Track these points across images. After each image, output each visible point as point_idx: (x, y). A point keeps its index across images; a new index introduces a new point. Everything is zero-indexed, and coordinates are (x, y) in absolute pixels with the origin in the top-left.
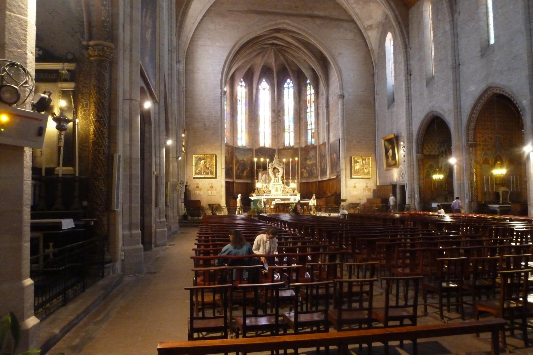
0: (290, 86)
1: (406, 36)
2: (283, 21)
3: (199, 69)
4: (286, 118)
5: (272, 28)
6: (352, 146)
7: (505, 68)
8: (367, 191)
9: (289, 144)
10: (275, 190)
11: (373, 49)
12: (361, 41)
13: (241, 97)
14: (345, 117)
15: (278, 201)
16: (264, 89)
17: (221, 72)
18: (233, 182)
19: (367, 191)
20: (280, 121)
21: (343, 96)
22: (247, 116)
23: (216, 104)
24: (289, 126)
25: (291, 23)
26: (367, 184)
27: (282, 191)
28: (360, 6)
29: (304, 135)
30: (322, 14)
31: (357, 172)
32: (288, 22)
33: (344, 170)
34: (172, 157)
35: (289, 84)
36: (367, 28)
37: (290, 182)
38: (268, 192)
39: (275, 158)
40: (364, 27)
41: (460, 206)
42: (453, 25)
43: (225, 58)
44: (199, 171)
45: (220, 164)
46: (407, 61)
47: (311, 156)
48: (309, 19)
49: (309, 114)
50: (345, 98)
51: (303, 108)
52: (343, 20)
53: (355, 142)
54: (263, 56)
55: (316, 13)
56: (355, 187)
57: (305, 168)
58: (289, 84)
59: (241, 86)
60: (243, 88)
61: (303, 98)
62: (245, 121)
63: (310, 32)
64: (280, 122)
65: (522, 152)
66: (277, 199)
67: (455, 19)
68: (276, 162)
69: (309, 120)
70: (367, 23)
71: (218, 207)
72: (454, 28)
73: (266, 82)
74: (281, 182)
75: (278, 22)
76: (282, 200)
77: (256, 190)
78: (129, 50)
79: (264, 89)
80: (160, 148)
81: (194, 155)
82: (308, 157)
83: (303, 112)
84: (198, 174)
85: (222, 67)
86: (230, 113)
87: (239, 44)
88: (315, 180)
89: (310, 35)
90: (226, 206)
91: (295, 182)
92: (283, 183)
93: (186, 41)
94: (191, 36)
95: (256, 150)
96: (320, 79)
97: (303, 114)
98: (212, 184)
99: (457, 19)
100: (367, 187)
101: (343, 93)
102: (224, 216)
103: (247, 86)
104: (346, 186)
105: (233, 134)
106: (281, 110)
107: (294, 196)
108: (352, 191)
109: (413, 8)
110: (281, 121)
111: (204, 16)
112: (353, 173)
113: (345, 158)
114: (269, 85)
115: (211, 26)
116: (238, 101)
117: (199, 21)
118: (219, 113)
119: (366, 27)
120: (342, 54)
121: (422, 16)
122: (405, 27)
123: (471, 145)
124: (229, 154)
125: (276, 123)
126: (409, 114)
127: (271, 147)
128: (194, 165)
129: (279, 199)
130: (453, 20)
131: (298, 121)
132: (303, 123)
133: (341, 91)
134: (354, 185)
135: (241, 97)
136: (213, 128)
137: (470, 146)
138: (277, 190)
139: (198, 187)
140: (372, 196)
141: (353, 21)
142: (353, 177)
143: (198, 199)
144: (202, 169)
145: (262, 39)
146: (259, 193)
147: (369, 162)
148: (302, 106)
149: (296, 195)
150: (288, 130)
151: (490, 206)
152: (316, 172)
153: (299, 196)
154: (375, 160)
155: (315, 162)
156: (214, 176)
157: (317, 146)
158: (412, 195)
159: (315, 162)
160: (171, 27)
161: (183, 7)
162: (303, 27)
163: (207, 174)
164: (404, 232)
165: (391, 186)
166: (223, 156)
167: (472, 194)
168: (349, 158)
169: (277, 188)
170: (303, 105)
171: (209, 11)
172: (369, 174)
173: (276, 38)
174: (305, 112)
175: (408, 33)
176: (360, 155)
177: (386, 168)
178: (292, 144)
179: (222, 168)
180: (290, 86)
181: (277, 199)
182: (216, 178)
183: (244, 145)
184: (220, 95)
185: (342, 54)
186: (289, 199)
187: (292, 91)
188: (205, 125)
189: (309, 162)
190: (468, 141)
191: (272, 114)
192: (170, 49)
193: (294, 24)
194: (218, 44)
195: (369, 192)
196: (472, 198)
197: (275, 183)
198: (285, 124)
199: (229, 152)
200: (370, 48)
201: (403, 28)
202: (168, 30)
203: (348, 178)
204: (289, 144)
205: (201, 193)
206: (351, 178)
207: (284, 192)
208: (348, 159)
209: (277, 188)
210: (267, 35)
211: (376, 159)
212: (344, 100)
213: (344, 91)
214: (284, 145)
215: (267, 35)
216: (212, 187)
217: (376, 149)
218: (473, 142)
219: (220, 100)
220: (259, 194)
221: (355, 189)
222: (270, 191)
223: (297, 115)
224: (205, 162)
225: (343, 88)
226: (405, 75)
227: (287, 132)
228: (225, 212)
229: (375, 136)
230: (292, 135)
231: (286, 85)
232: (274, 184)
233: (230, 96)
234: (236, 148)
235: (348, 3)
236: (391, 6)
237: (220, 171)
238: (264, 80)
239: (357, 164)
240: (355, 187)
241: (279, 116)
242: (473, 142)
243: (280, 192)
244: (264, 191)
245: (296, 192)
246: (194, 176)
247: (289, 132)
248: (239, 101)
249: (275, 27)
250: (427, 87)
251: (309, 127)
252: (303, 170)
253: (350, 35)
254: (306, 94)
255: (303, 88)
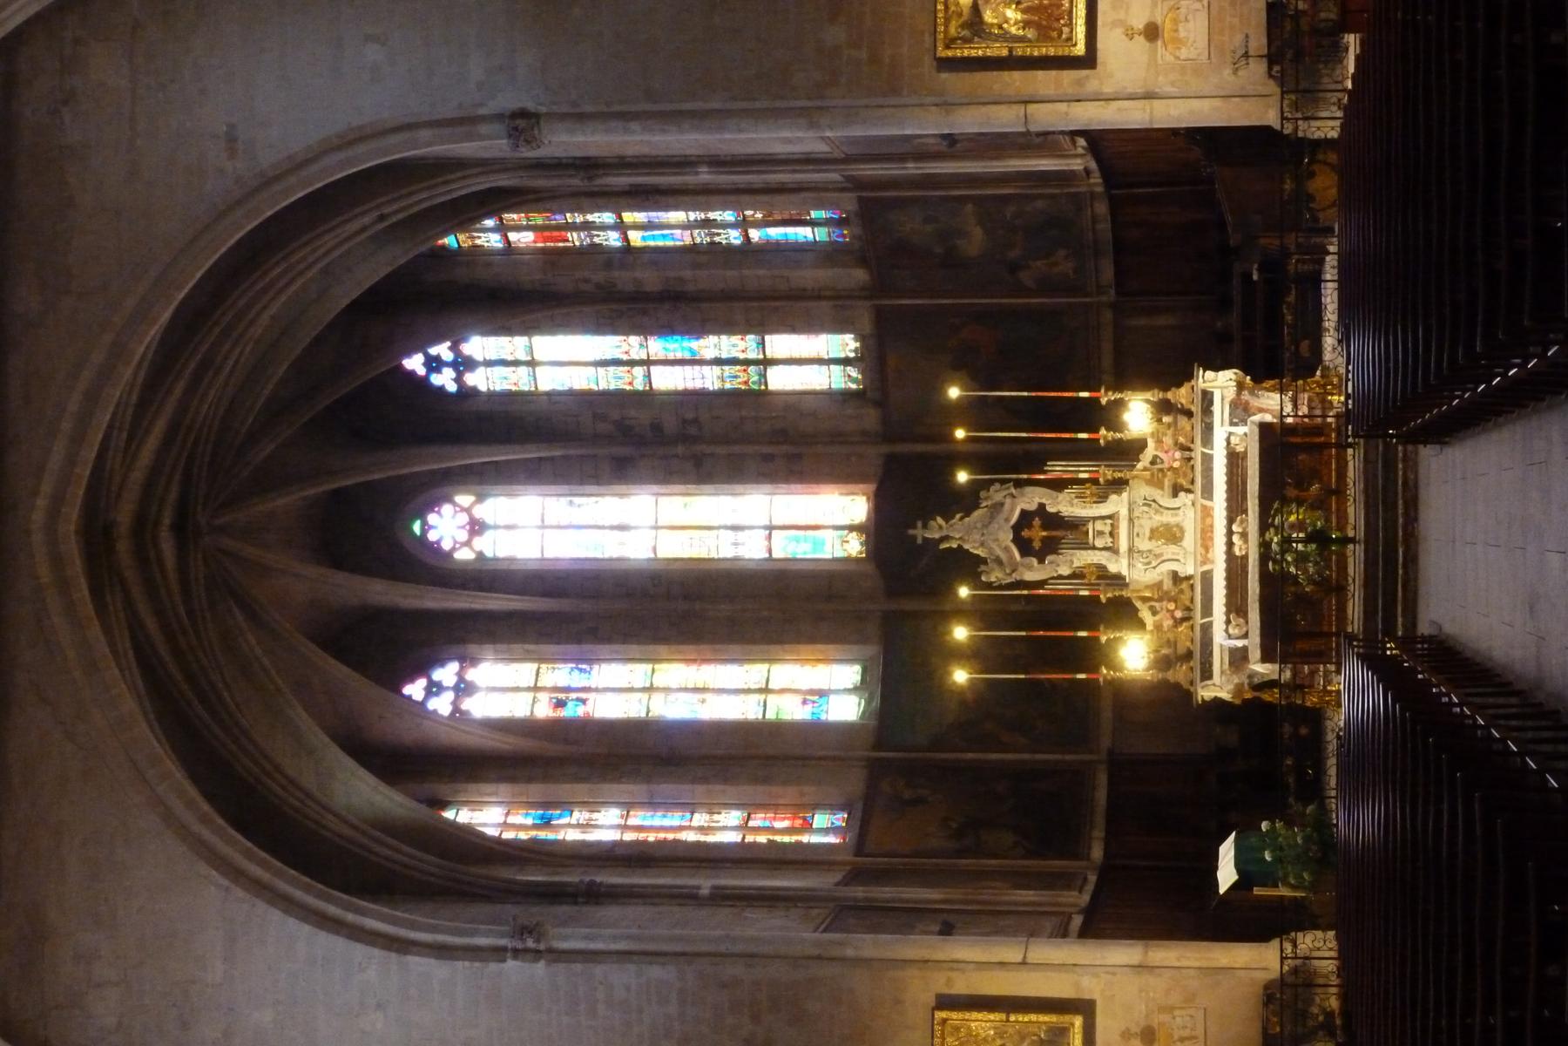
2: (38, 538)
6: (864, 54)
13: (536, 689)
15: (1244, 535)
21: (521, 123)
22: (662, 650)
23: (601, 994)
25: (47, 487)
27: (1175, 495)
29: (786, 273)
31: (1047, 20)
33: (1032, 108)
35: (434, 364)
38: (1185, 598)
39: (946, 538)
45: (1002, 975)
47: (929, 228)
50: (530, 106)
51: (600, 277)
53: (835, 34)
56: (1152, 32)
57: (1014, 268)
58: (434, 364)
60: (472, 675)
62: (693, 668)
65: (950, 682)
69: (683, 238)
73: (432, 518)
75: (44, 573)
79: (476, 527)
82: (938, 250)
83: (624, 279)
86: (648, 780)
88: (1102, 208)
90: (1275, 943)
91: (1119, 405)
92: (1118, 485)
95: (891, 593)
97: (638, 274)
104: (1149, 96)
110: (690, 416)
112: (1052, 52)
113: (947, 105)
118: (656, 972)
125: (708, 449)
132: (705, 279)
133: (484, 129)
134: (1140, 40)
135: (536, 689)
136: (756, 1018)
138: (1172, 535)
148: (586, 281)
149: (1207, 397)
150: (752, 369)
152: (1040, 204)
153: (1210, 374)
155: (969, 207)
156: (1078, 1021)
157: (860, 199)
159: (969, 207)
166: (940, 956)
168: (944, 76)
169: (1154, 534)
170: (578, 275)
179: (1024, 963)
181: (1230, 544)
182: (1085, 1008)
184: (541, 965)
189: (974, 241)
197: (1123, 545)
199: (907, 794)
203: (1091, 81)
206: (1089, 60)
207: (1183, 482)
208: (953, 81)
209: (1154, 534)
212: (543, 109)
213: (483, 111)
219: (578, 967)
220: (1196, 662)
223: (645, 312)
225: (462, 121)
227: (763, 376)
232: (1131, 550)
233: (530, 780)
234: (879, 745)
239: (989, 16)
240: (1152, 32)
241: (657, 428)
243: (1185, 513)
244: (1178, 622)
245: (1181, 395)
252: (1026, 277)
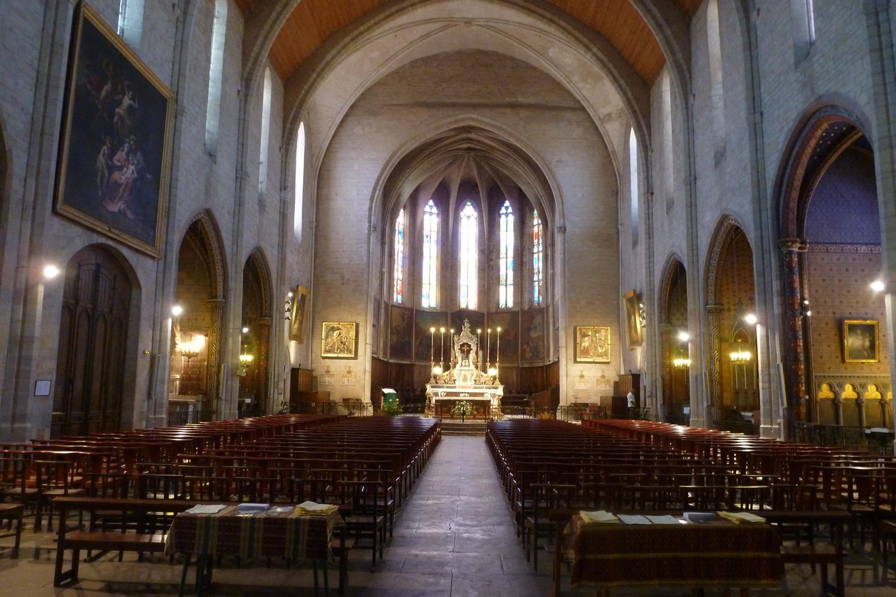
0: (509, 211)
1: (645, 132)
2: (468, 115)
3: (337, 195)
4: (502, 263)
5: (451, 127)
7: (737, 185)
8: (603, 384)
9: (506, 304)
10: (461, 379)
11: (615, 151)
12: (595, 139)
14: (566, 262)
15: (465, 396)
16: (469, 217)
17: (369, 198)
18: (412, 366)
19: (603, 384)
20: (492, 267)
21: (563, 229)
22: (439, 261)
24: (507, 275)
25: (480, 118)
26: (603, 371)
28: (589, 86)
30: (531, 100)
31: (585, 352)
32: (476, 116)
34: (234, 329)
35: (507, 208)
36: (604, 118)
37: (488, 366)
40: (599, 118)
41: (346, 408)
42: (688, 114)
43: (376, 177)
44: (331, 347)
45: (364, 338)
46: (648, 171)
48: (508, 111)
49: (535, 256)
50: (567, 231)
51: (527, 247)
52: (564, 109)
53: (583, 303)
54: (459, 168)
55: (522, 100)
56: (582, 376)
57: (528, 344)
58: (507, 208)
59: (431, 214)
60: (434, 216)
61: (527, 230)
63: (510, 130)
64: (493, 269)
66: (462, 393)
67: (690, 106)
68: (465, 334)
69: (535, 266)
70: (603, 111)
71: (358, 404)
72: (688, 120)
73: (471, 207)
74: (472, 367)
75: (459, 117)
76: (471, 394)
77: (432, 379)
78: (31, 208)
79: (469, 217)
80: (167, 318)
81: (324, 323)
83: (526, 253)
84: (329, 351)
85: (371, 190)
86: (409, 257)
87: (398, 154)
88: (541, 364)
89: (511, 134)
92: (477, 367)
93: (319, 153)
94: (327, 145)
95: (452, 314)
96: (126, 252)
97: (527, 256)
98: (349, 367)
99: (692, 105)
100: (603, 377)
101: (564, 224)
102: (367, 418)
103: (440, 213)
105: (414, 288)
106: (494, 250)
107: (494, 390)
108: (577, 384)
109: (654, 86)
111: (347, 116)
113: (566, 329)
114: (476, 211)
115: (358, 130)
116: (425, 237)
117: (338, 123)
118: (365, 258)
119: (602, 117)
120: (563, 162)
121: (662, 99)
122: (644, 117)
123: (709, 310)
124: (403, 320)
125: (486, 271)
126: (649, 258)
127: (477, 310)
128: (323, 338)
129: (466, 394)
130: (687, 108)
131: (519, 267)
136: (354, 281)
137: (710, 312)
138: (465, 379)
139: (328, 372)
140: (612, 392)
141: (583, 109)
142: (578, 360)
143: (328, 390)
144: (334, 344)
145: (442, 144)
146: (437, 383)
147: (606, 336)
149: (497, 388)
150: (505, 282)
151: (743, 414)
154: (618, 333)
156: (353, 356)
157: (544, 308)
158: (654, 393)
160: (243, 145)
161: (295, 108)
162: (499, 124)
163: (342, 351)
164: (885, 466)
165: (631, 377)
167: (712, 393)
169: (465, 376)
171: (352, 107)
172: (607, 355)
173: (470, 140)
174: (529, 253)
175: (649, 126)
176: (592, 324)
177: (629, 346)
178: (510, 304)
179: (366, 344)
180: (509, 211)
181: (462, 393)
182: (356, 358)
183: (433, 305)
185: (563, 162)
186: (482, 394)
187: (511, 218)
188: (343, 278)
189: (534, 334)
190: (707, 304)
191: (479, 256)
192: (239, 176)
193: (488, 120)
194: (366, 157)
195: (608, 386)
196: (711, 400)
197: (462, 368)
198: (501, 273)
200: (610, 151)
201: (640, 117)
202: (238, 150)
203: (571, 362)
204: (506, 304)
205: (332, 380)
206: (575, 362)
209: (465, 376)
210: (449, 137)
211: (619, 331)
212: (566, 234)
213: (566, 220)
214: (499, 307)
215: (449, 137)
216: (349, 372)
217: (619, 314)
218: (713, 306)
220: (435, 384)
221: (582, 380)
222: (455, 380)
223: (518, 257)
224: (340, 334)
226: (644, 194)
227: (503, 285)
228: (369, 412)
229: (619, 292)
230: (511, 289)
231: (503, 210)
235: (571, 81)
236: (620, 86)
237: (364, 347)
238: (469, 203)
239: (586, 338)
240: (582, 376)
241: (492, 260)
242: (713, 306)
245: (497, 382)
246: (323, 355)
247: (506, 286)
248: (427, 237)
249: (461, 125)
250: (667, 213)
251: (536, 278)
252: (525, 346)
253: (578, 132)
254: (533, 223)
255: (528, 215)
